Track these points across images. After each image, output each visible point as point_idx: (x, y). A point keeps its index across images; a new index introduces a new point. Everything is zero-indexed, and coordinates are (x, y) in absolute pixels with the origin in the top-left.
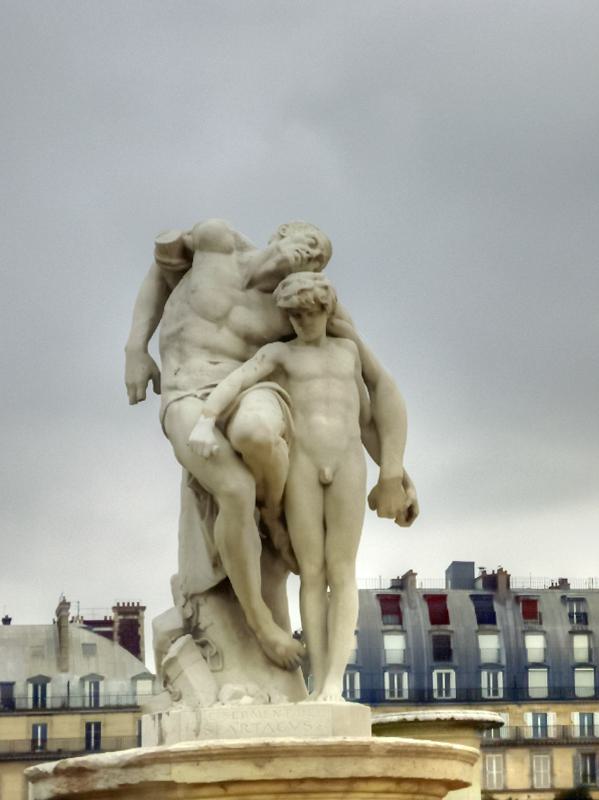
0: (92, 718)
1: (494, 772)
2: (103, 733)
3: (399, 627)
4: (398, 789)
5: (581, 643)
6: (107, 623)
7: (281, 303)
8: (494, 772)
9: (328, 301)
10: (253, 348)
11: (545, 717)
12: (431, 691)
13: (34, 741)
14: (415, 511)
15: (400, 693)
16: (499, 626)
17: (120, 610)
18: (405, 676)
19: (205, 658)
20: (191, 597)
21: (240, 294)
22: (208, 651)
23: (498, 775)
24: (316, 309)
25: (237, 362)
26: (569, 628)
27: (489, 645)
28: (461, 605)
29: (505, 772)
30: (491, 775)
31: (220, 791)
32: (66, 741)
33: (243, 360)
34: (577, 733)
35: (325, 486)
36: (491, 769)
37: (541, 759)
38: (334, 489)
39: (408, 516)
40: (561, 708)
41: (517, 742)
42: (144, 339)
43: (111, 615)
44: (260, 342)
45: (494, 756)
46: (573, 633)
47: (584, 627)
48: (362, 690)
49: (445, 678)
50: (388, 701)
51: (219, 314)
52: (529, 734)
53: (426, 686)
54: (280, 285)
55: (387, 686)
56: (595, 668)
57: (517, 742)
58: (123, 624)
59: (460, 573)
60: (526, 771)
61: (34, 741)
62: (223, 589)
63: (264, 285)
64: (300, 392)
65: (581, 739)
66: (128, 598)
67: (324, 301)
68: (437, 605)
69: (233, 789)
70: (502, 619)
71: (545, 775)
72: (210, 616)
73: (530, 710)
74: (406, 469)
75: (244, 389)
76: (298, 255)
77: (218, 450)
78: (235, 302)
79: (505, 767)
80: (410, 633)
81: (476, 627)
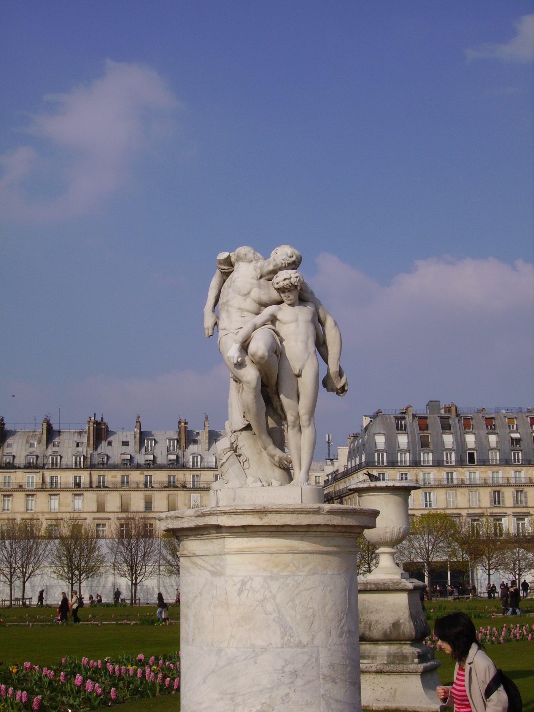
0: (195, 473)
1: (451, 500)
2: (153, 479)
3: (404, 432)
4: (484, 510)
5: (493, 439)
7: (277, 286)
8: (451, 500)
10: (262, 308)
11: (452, 474)
12: (443, 461)
13: (170, 482)
15: (383, 463)
16: (452, 431)
18: (453, 454)
21: (255, 281)
23: (453, 501)
25: (253, 315)
26: (487, 431)
27: (448, 440)
28: (434, 422)
29: (456, 499)
30: (450, 501)
33: (257, 314)
34: (445, 482)
36: (450, 498)
37: (451, 492)
40: (483, 469)
41: (462, 485)
42: (213, 305)
44: (266, 305)
45: (451, 492)
46: (488, 433)
47: (494, 431)
48: (388, 461)
49: (428, 458)
50: (400, 466)
51: (246, 292)
52: (467, 482)
53: (418, 459)
54: (275, 277)
55: (376, 460)
56: (499, 450)
57: (462, 485)
59: (433, 405)
60: (467, 499)
61: (170, 482)
63: (267, 277)
65: (515, 483)
68: (423, 423)
70: (453, 428)
71: (476, 501)
73: (423, 471)
75: (255, 329)
76: (283, 262)
79: (456, 497)
80: (409, 432)
81: (441, 432)
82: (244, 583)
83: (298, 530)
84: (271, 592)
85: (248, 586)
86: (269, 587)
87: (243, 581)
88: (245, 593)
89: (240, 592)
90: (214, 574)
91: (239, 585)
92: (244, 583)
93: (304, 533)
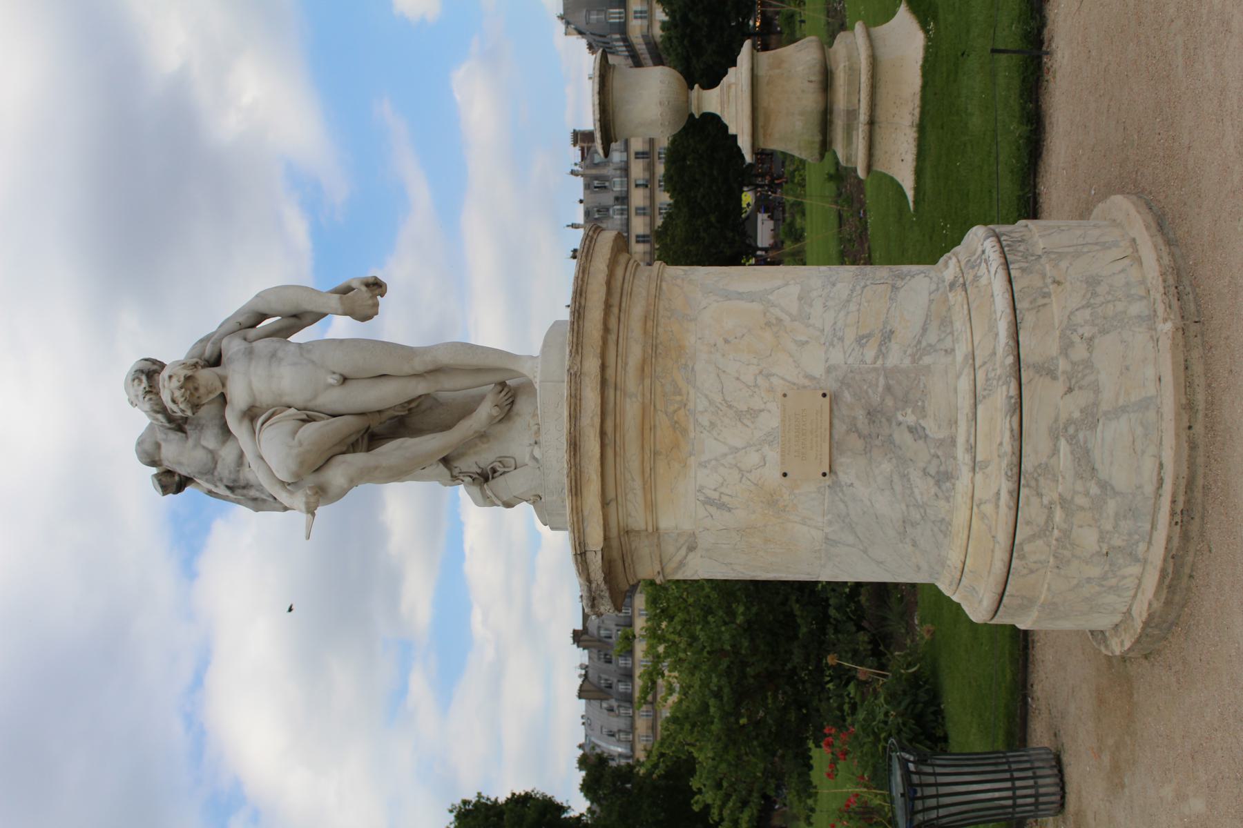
6: (582, 150)
9: (183, 373)
14: (371, 281)
17: (575, 144)
19: (504, 473)
20: (454, 478)
21: (191, 442)
22: (501, 470)
24: (190, 385)
31: (613, 506)
32: (645, 197)
35: (345, 379)
38: (346, 372)
39: (376, 286)
43: (578, 148)
51: (210, 456)
58: (583, 141)
62: (446, 461)
64: (265, 398)
66: (569, 139)
67: (182, 379)
69: (611, 494)
72: (469, 464)
74: (331, 288)
77: (310, 488)
78: (197, 444)
82: (709, 502)
83: (619, 284)
84: (725, 455)
85: (715, 495)
86: (716, 459)
87: (704, 503)
88: (725, 499)
89: (722, 506)
90: (691, 549)
91: (713, 510)
92: (709, 502)
93: (618, 393)
